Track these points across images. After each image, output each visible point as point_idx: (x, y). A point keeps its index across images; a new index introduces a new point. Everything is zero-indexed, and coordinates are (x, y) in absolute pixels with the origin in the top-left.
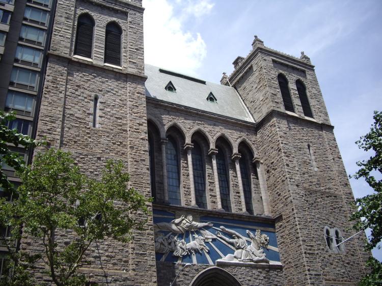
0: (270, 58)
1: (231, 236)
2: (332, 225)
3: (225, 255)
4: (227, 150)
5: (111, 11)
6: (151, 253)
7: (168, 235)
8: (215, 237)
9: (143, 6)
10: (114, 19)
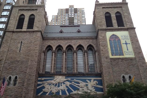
0: (101, 7)
1: (78, 83)
2: (127, 73)
3: (75, 91)
4: (92, 48)
5: (112, 8)
7: (51, 85)
8: (71, 84)
9: (127, 2)
10: (32, 13)
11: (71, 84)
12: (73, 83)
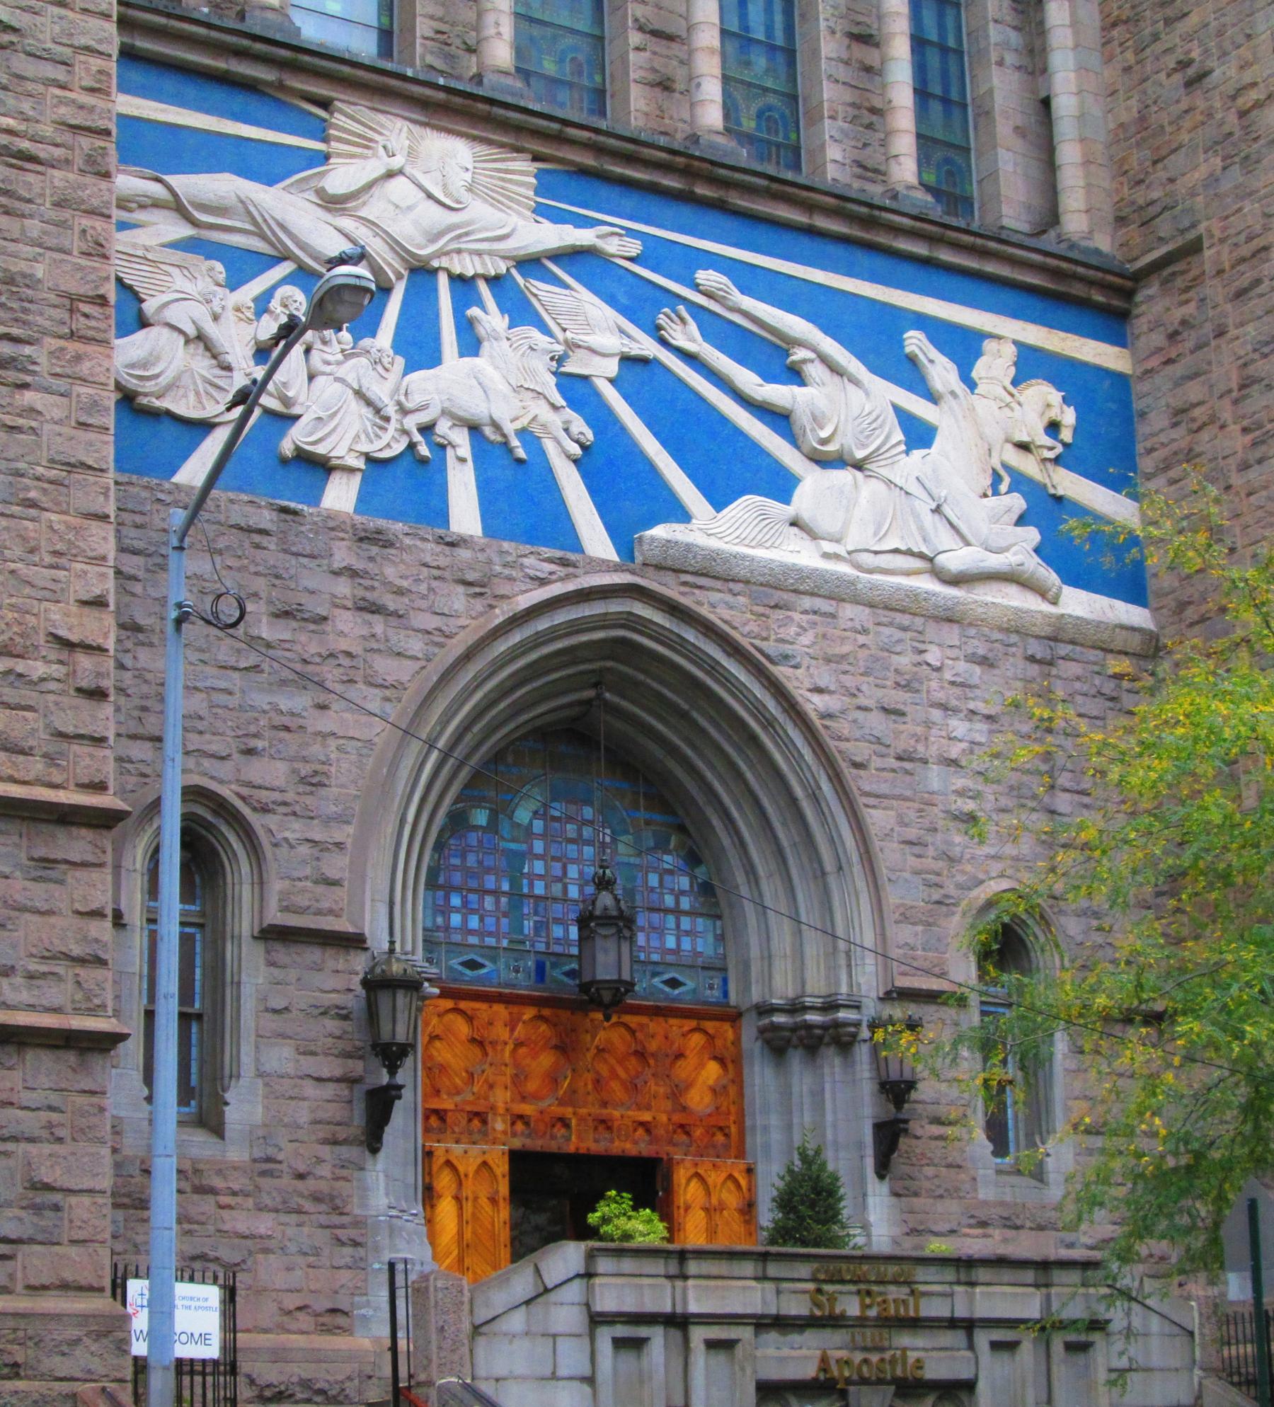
6: (78, 358)
11: (646, 346)
12: (688, 336)
